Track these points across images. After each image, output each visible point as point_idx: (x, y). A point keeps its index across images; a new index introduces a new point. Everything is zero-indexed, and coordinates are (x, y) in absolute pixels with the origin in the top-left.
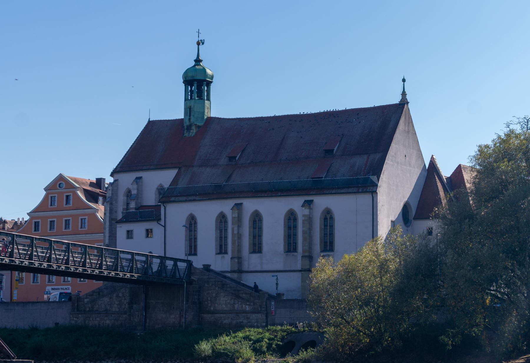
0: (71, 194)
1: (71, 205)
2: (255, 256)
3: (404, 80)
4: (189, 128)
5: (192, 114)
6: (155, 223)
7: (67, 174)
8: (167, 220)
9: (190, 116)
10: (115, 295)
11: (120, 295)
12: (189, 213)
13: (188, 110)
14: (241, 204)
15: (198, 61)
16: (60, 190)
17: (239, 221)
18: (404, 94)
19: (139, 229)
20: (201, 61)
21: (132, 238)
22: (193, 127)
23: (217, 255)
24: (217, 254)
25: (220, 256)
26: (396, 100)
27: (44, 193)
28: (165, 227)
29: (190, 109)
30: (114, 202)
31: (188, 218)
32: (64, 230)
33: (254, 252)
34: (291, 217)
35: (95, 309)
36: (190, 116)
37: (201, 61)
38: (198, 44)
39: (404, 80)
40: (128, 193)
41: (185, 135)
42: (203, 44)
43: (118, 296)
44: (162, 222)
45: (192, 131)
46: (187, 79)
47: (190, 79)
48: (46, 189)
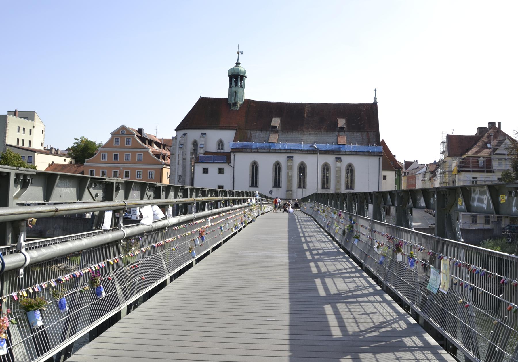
0: (131, 138)
1: (131, 145)
2: (300, 190)
3: (375, 90)
5: (236, 96)
6: (227, 165)
7: (127, 125)
8: (235, 163)
9: (235, 97)
12: (253, 160)
13: (233, 93)
14: (292, 157)
15: (238, 64)
16: (122, 135)
17: (290, 168)
18: (375, 98)
19: (213, 168)
20: (240, 64)
21: (223, 173)
23: (273, 188)
24: (273, 187)
26: (371, 101)
27: (110, 136)
28: (234, 168)
29: (235, 93)
30: (185, 148)
31: (274, 163)
32: (125, 161)
33: (300, 187)
34: (326, 168)
36: (235, 97)
37: (240, 64)
38: (238, 53)
39: (375, 90)
40: (195, 144)
41: (231, 109)
42: (242, 54)
44: (232, 164)
45: (236, 107)
46: (230, 74)
47: (236, 74)
48: (112, 134)
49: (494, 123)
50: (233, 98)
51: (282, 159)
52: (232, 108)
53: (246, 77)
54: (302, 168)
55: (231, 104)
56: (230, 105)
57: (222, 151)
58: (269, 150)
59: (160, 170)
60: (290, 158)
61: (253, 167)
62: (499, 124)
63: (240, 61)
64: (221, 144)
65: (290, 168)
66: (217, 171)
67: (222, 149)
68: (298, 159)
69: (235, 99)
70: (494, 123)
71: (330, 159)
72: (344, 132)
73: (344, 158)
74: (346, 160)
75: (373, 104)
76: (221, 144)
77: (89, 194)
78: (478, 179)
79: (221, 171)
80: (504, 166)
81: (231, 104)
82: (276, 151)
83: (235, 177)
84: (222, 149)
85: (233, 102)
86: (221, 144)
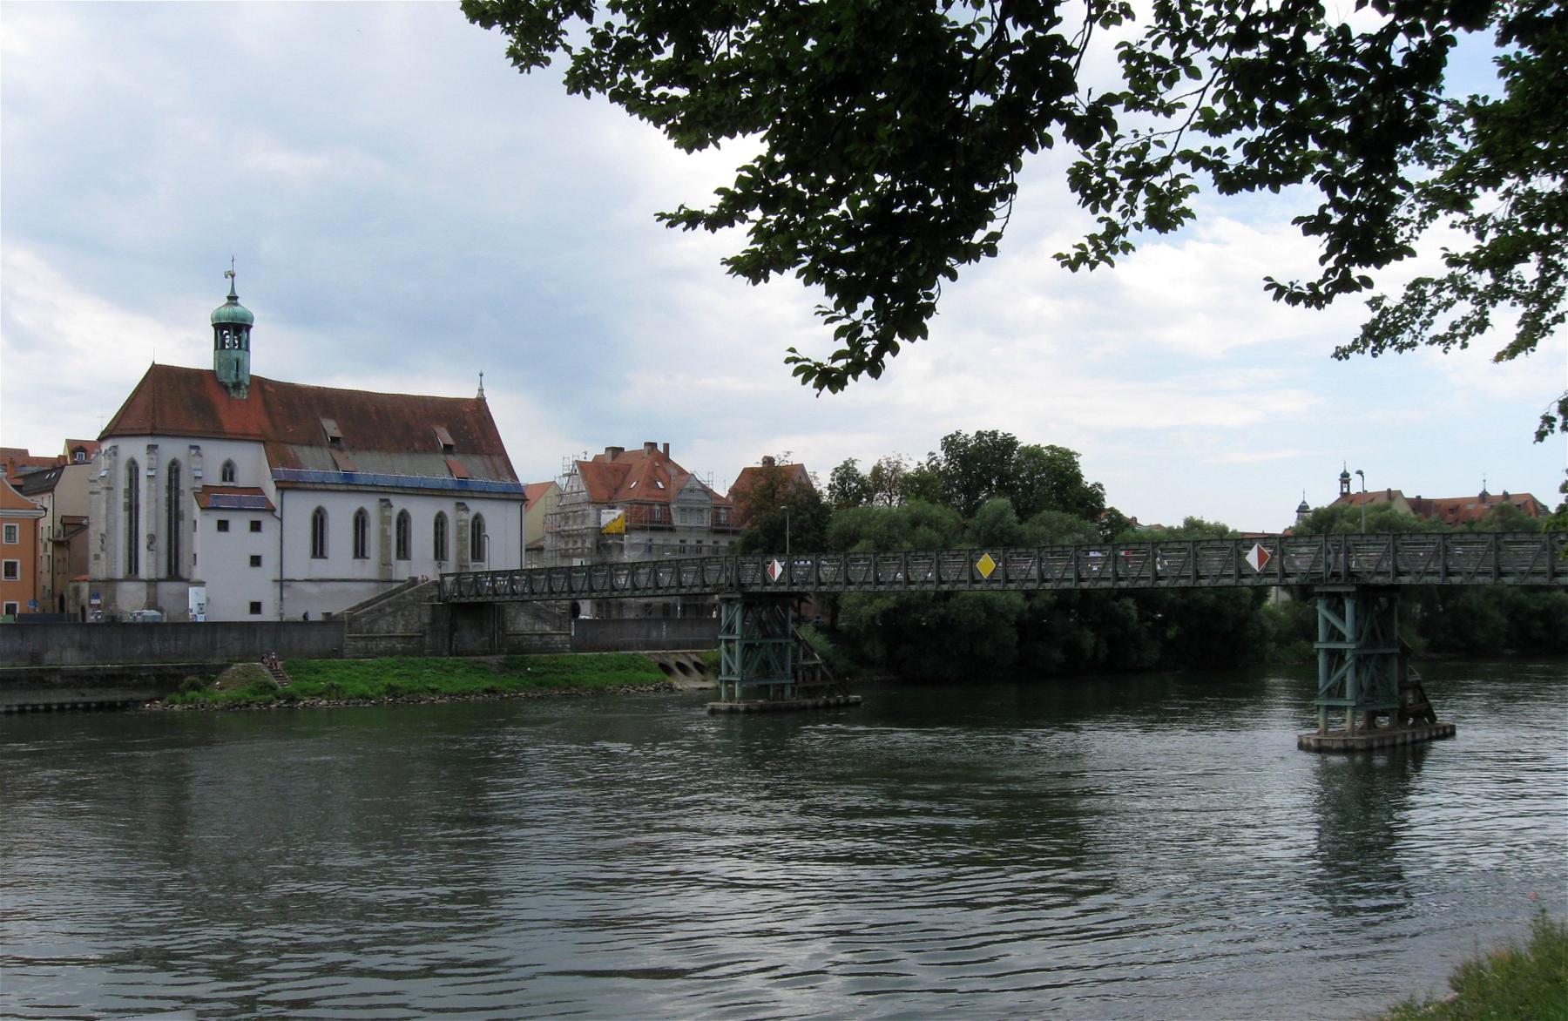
2: (403, 562)
3: (481, 375)
4: (237, 386)
10: (400, 613)
11: (407, 613)
15: (233, 299)
18: (481, 390)
22: (243, 387)
25: (358, 562)
28: (281, 520)
34: (440, 521)
35: (375, 630)
37: (236, 298)
39: (481, 375)
40: (174, 468)
43: (403, 615)
44: (278, 514)
49: (655, 444)
50: (234, 372)
51: (371, 505)
52: (234, 394)
53: (1389, 490)
54: (404, 519)
55: (230, 385)
56: (226, 387)
57: (231, 484)
58: (349, 484)
59: (32, 522)
60: (387, 504)
61: (315, 520)
62: (666, 446)
63: (246, 304)
64: (228, 471)
65: (385, 521)
66: (248, 526)
67: (231, 479)
68: (398, 504)
69: (237, 376)
70: (655, 444)
71: (448, 507)
72: (453, 453)
73: (469, 504)
74: (475, 507)
75: (477, 398)
76: (228, 469)
77: (332, 577)
78: (704, 543)
79: (256, 526)
80: (688, 520)
81: (230, 385)
82: (512, 497)
83: (285, 539)
84: (231, 479)
85: (234, 380)
86: (228, 469)
